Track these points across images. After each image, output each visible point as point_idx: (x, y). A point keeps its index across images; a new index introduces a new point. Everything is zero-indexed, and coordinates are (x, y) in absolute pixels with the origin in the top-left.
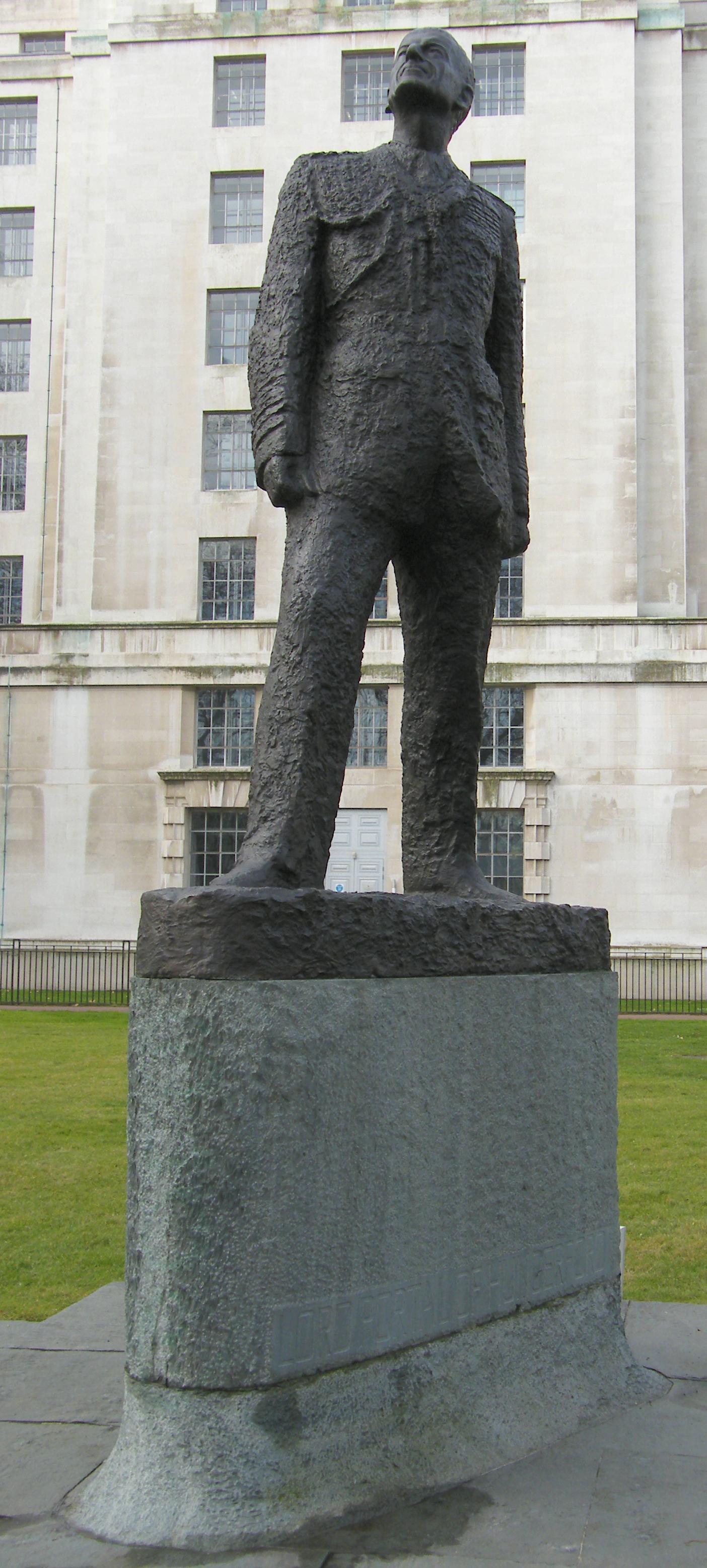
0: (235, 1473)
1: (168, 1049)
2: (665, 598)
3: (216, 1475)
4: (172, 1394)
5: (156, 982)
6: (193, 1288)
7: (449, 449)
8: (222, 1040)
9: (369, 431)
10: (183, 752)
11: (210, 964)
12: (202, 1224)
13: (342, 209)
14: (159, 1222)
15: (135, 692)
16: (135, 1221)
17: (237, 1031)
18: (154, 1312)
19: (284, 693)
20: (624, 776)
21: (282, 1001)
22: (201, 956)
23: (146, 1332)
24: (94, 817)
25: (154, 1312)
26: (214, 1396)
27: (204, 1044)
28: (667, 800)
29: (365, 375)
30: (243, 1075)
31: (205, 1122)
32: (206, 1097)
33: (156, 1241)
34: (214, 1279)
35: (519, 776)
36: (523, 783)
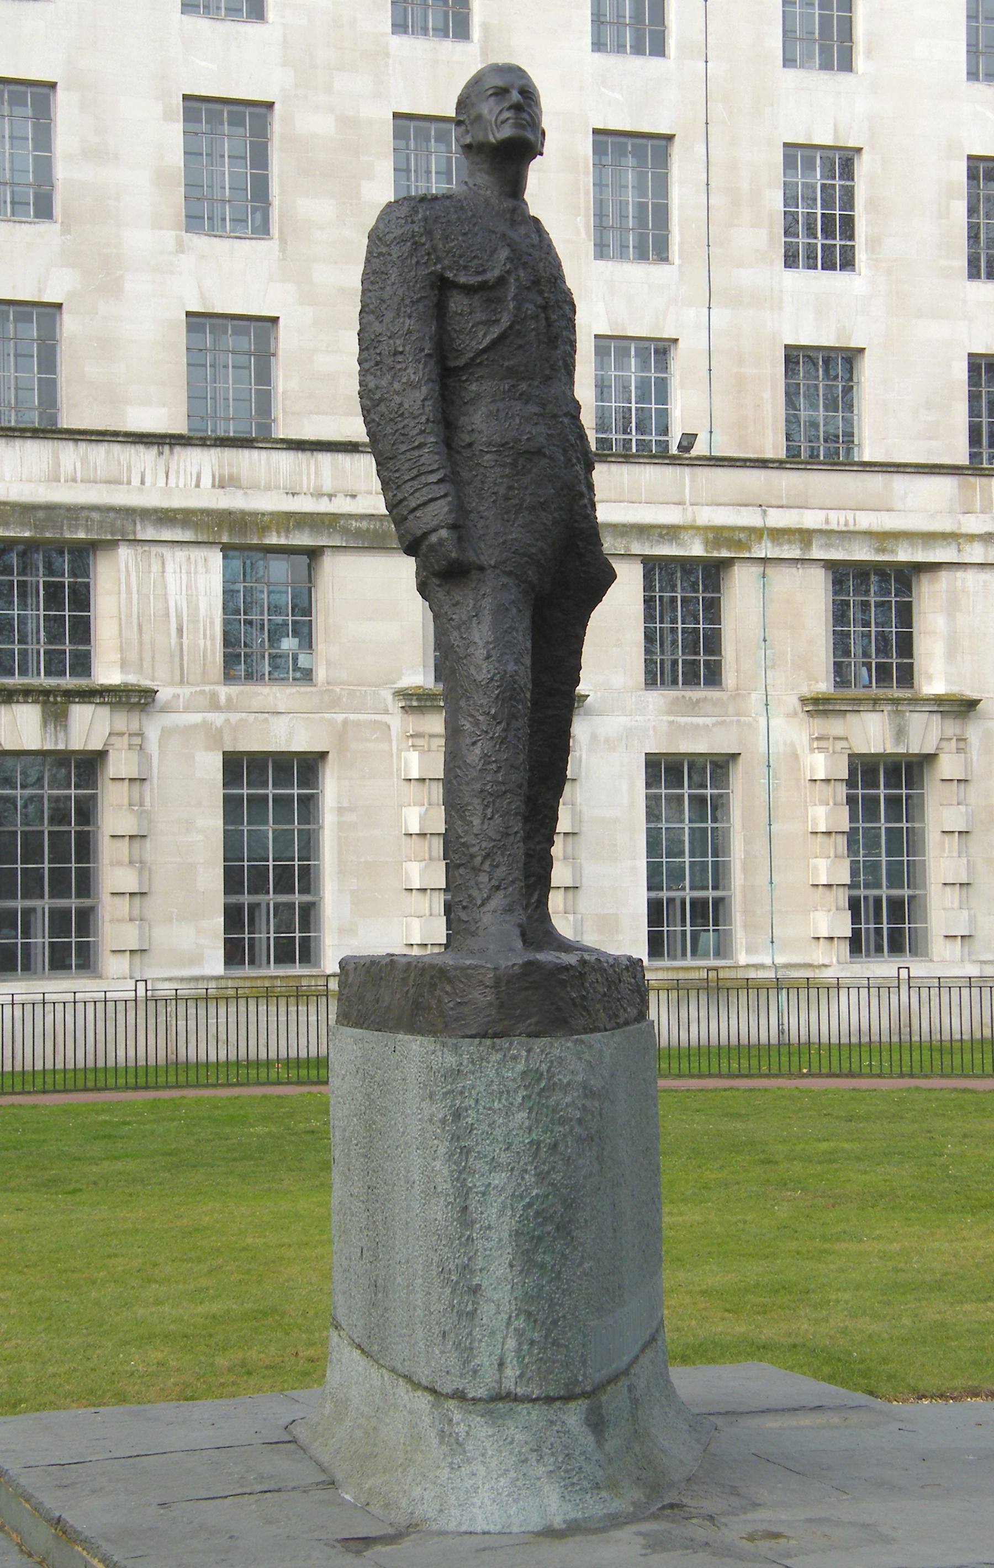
0: (580, 1468)
1: (503, 1101)
3: (566, 1471)
4: (521, 1406)
5: (488, 1042)
6: (539, 1311)
7: (576, 521)
8: (554, 1090)
9: (521, 505)
11: (537, 1023)
12: (544, 1253)
13: (465, 267)
14: (501, 1256)
16: (470, 1259)
17: (565, 1081)
18: (499, 1336)
19: (494, 766)
22: (529, 1017)
23: (490, 1355)
25: (499, 1336)
26: (558, 1404)
27: (539, 1094)
29: (512, 448)
30: (571, 1120)
31: (544, 1163)
32: (544, 1140)
33: (499, 1273)
34: (556, 1300)
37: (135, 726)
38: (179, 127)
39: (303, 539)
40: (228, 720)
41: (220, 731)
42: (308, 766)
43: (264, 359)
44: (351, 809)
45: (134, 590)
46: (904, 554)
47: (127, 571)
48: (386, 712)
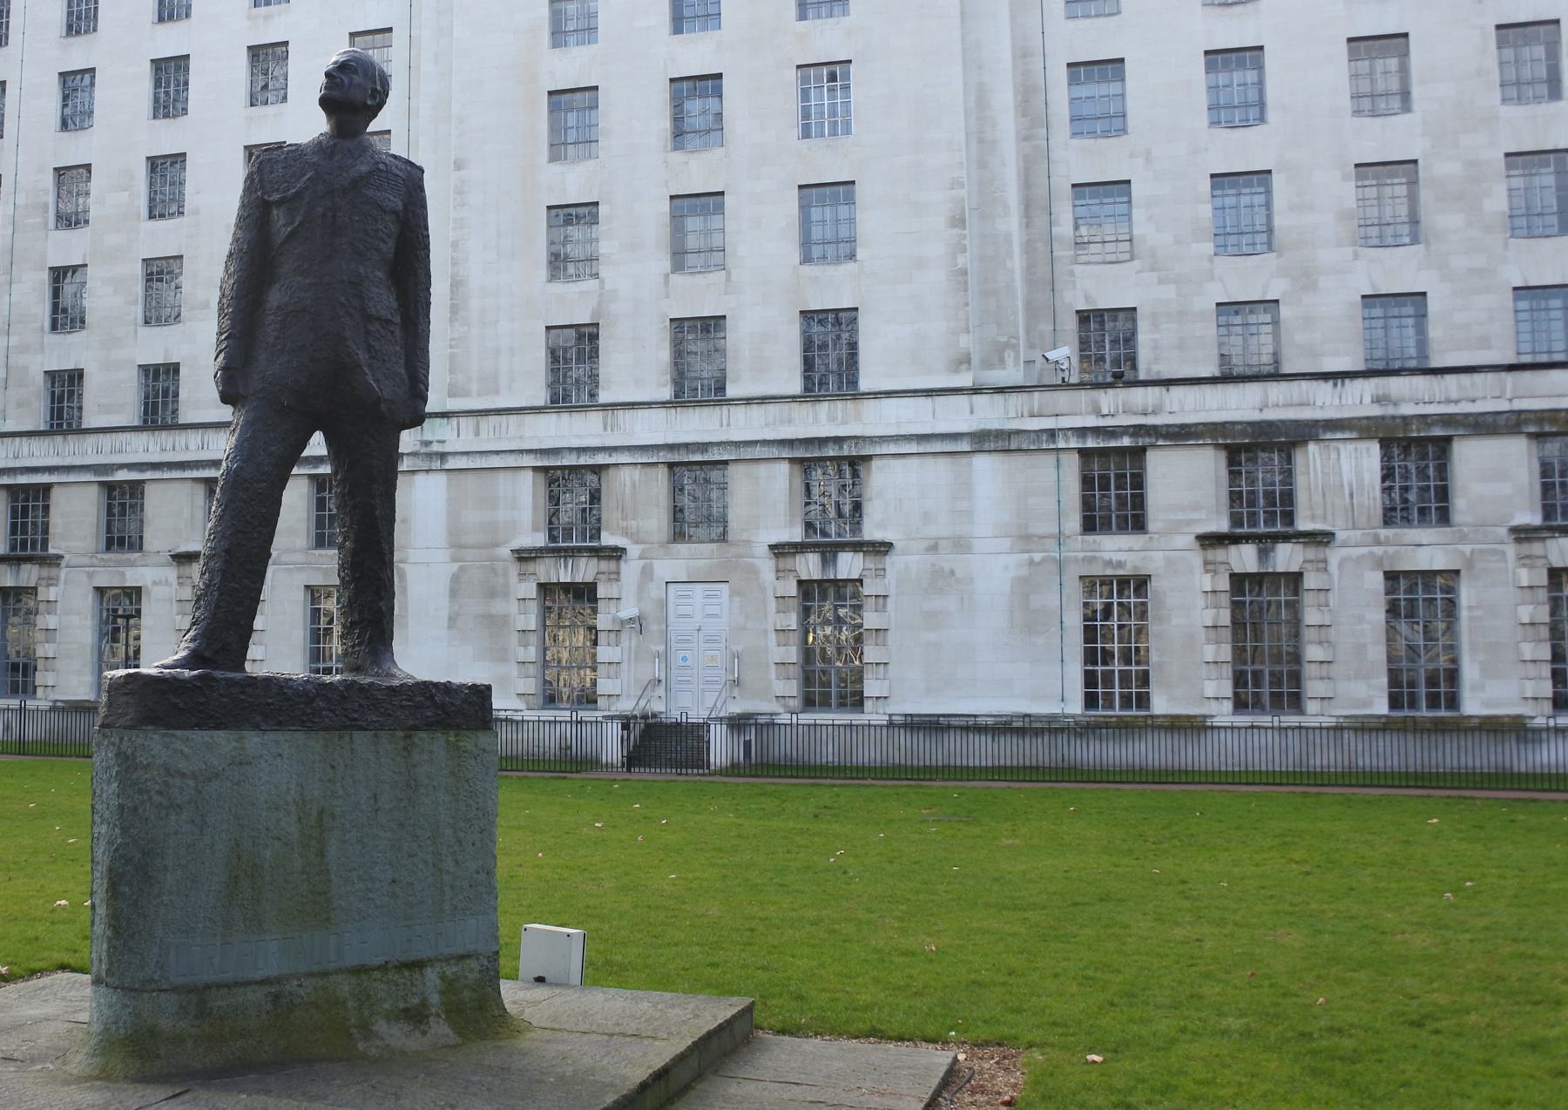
10: (535, 529)
15: (485, 474)
20: (961, 545)
21: (179, 745)
24: (454, 593)
28: (1006, 568)
35: (857, 547)
37: (1321, 556)
39: (1438, 432)
43: (1421, 316)
44: (1477, 607)
46: (601, 459)
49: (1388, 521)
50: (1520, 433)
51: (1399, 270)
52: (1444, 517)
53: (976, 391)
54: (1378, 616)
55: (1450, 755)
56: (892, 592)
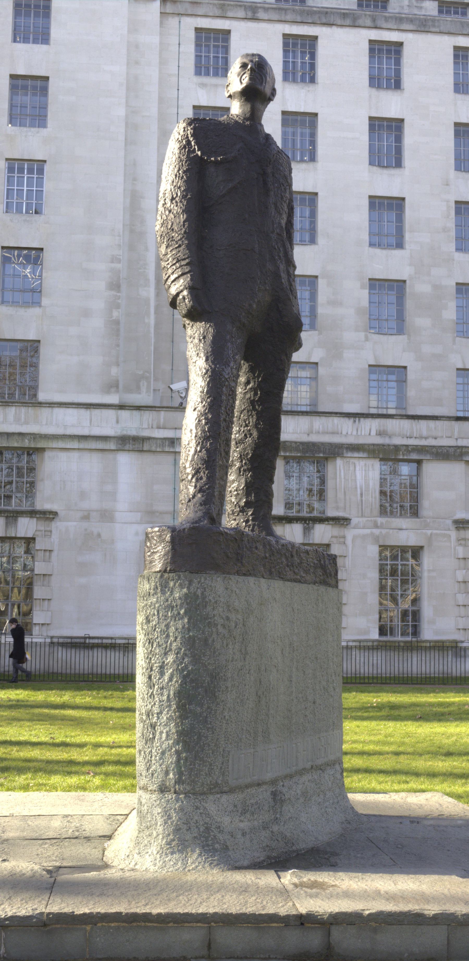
2: (138, 389)
20: (107, 516)
28: (137, 534)
35: (33, 513)
36: (35, 519)
37: (342, 534)
38: (367, 291)
39: (414, 456)
40: (381, 532)
41: (378, 537)
42: (416, 552)
43: (402, 381)
45: (343, 477)
47: (340, 469)
48: (449, 530)
49: (383, 511)
50: (462, 460)
51: (391, 350)
52: (415, 512)
53: (121, 407)
54: (374, 575)
55: (417, 664)
56: (56, 548)
